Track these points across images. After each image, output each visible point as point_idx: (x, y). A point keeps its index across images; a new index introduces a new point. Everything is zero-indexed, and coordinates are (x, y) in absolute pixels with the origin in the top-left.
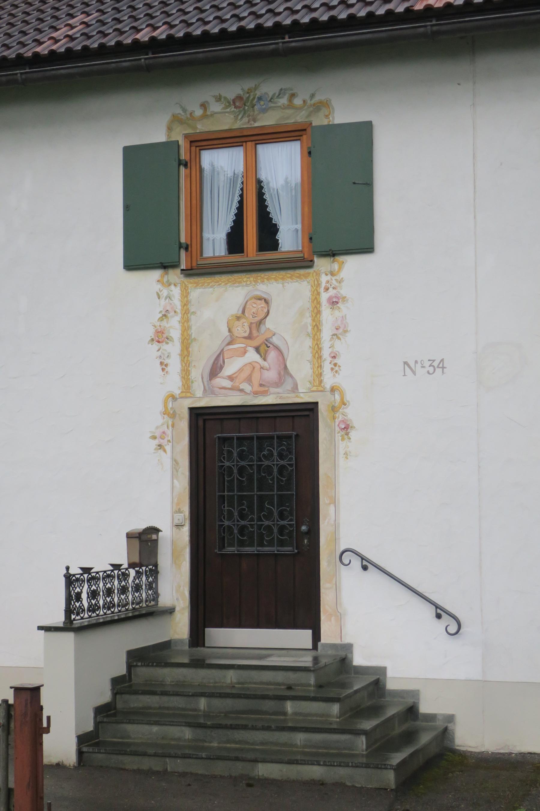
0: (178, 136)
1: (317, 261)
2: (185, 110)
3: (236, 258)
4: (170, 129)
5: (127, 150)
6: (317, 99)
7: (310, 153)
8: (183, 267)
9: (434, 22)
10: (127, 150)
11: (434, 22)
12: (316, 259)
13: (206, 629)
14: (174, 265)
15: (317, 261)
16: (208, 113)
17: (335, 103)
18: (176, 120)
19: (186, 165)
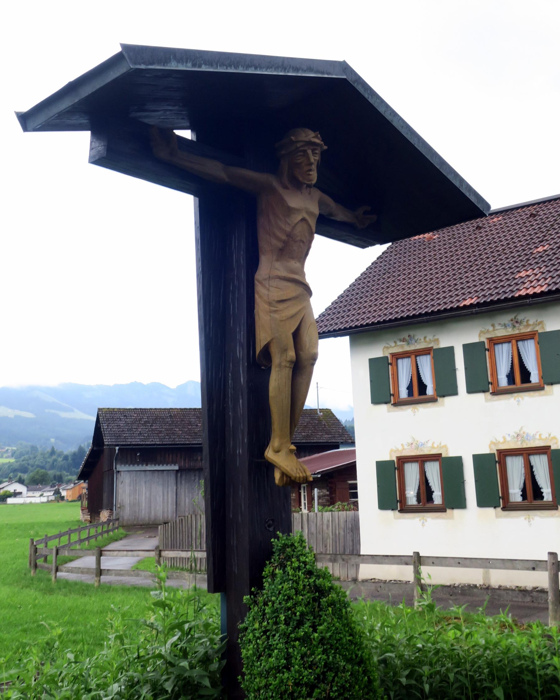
0: (483, 339)
1: (546, 387)
2: (485, 329)
3: (411, 399)
4: (480, 336)
5: (371, 361)
6: (538, 321)
7: (538, 343)
8: (491, 391)
9: (531, 300)
10: (371, 361)
11: (531, 300)
12: (438, 398)
13: (361, 554)
14: (488, 391)
15: (546, 387)
16: (495, 329)
17: (440, 340)
18: (482, 332)
19: (488, 351)
